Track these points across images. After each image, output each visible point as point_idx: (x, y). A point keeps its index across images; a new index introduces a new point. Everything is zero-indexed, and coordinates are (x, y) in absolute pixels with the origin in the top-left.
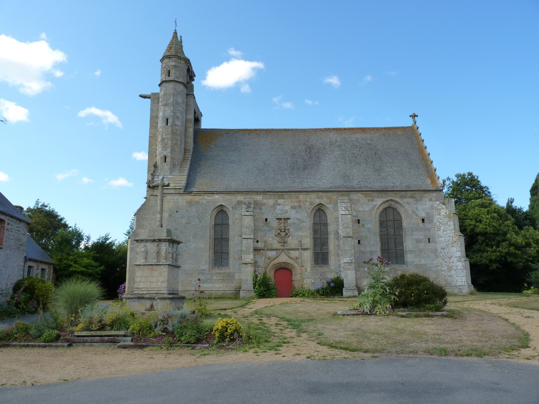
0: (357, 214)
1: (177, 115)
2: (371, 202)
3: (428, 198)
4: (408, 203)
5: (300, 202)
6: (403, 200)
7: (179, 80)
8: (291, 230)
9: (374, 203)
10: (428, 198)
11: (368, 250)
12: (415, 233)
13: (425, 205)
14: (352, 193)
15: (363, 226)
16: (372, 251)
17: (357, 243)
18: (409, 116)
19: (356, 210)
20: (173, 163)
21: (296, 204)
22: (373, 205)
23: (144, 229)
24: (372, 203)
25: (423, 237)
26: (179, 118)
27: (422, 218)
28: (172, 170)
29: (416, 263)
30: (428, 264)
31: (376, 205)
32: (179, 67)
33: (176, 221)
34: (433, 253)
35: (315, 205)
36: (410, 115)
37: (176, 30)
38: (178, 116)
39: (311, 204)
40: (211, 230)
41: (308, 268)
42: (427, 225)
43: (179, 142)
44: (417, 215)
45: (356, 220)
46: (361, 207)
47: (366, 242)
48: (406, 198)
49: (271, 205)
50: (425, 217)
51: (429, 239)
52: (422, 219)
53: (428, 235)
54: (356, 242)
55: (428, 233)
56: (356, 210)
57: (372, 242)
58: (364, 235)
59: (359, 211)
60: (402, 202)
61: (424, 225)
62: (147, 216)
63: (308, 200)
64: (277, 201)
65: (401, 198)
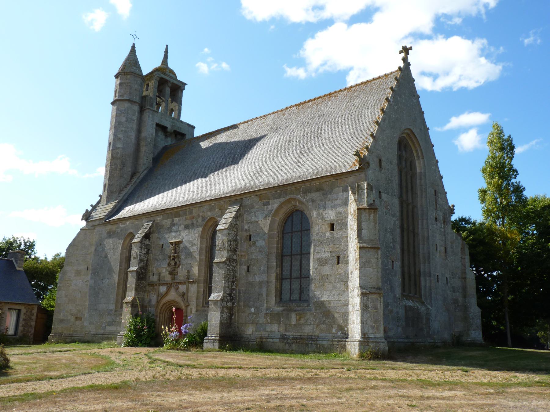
0: (249, 227)
1: (119, 137)
2: (266, 207)
3: (342, 187)
4: (313, 201)
5: (193, 218)
6: (306, 197)
7: (123, 97)
8: (182, 257)
9: (270, 207)
10: (342, 187)
11: (257, 280)
12: (319, 248)
13: (337, 199)
14: (245, 196)
15: (254, 244)
16: (262, 281)
17: (245, 271)
18: (399, 52)
19: (249, 220)
20: (110, 191)
21: (189, 222)
22: (268, 210)
23: (72, 266)
24: (267, 208)
25: (328, 254)
26: (121, 140)
27: (329, 223)
28: (109, 198)
29: (315, 300)
30: (333, 301)
31: (272, 210)
32: (125, 83)
33: (98, 255)
34: (342, 281)
35: (207, 219)
36: (115, 76)
37: (134, 44)
38: (120, 138)
39: (203, 218)
40: (124, 263)
41: (193, 308)
42: (337, 234)
43: (119, 166)
44: (323, 219)
45: (248, 235)
46: (254, 215)
47: (256, 268)
48: (310, 193)
49: (168, 227)
50: (334, 220)
51: (338, 257)
52: (329, 225)
53: (336, 250)
54: (244, 269)
55: (337, 248)
56: (249, 220)
57: (263, 269)
58: (254, 258)
59: (251, 223)
60: (304, 200)
61: (331, 234)
62: (75, 252)
63: (201, 214)
64: (173, 221)
65: (304, 193)
